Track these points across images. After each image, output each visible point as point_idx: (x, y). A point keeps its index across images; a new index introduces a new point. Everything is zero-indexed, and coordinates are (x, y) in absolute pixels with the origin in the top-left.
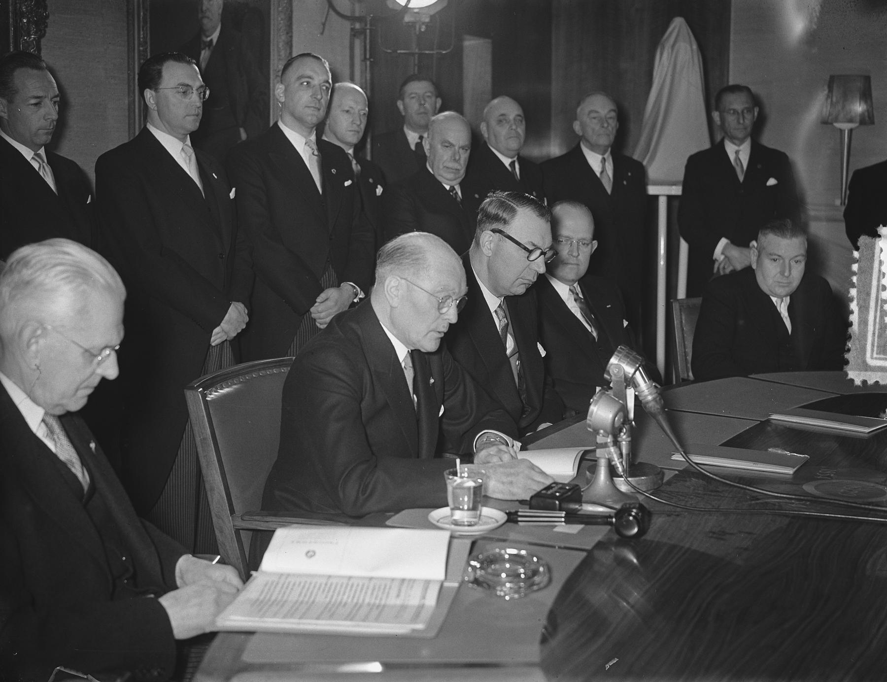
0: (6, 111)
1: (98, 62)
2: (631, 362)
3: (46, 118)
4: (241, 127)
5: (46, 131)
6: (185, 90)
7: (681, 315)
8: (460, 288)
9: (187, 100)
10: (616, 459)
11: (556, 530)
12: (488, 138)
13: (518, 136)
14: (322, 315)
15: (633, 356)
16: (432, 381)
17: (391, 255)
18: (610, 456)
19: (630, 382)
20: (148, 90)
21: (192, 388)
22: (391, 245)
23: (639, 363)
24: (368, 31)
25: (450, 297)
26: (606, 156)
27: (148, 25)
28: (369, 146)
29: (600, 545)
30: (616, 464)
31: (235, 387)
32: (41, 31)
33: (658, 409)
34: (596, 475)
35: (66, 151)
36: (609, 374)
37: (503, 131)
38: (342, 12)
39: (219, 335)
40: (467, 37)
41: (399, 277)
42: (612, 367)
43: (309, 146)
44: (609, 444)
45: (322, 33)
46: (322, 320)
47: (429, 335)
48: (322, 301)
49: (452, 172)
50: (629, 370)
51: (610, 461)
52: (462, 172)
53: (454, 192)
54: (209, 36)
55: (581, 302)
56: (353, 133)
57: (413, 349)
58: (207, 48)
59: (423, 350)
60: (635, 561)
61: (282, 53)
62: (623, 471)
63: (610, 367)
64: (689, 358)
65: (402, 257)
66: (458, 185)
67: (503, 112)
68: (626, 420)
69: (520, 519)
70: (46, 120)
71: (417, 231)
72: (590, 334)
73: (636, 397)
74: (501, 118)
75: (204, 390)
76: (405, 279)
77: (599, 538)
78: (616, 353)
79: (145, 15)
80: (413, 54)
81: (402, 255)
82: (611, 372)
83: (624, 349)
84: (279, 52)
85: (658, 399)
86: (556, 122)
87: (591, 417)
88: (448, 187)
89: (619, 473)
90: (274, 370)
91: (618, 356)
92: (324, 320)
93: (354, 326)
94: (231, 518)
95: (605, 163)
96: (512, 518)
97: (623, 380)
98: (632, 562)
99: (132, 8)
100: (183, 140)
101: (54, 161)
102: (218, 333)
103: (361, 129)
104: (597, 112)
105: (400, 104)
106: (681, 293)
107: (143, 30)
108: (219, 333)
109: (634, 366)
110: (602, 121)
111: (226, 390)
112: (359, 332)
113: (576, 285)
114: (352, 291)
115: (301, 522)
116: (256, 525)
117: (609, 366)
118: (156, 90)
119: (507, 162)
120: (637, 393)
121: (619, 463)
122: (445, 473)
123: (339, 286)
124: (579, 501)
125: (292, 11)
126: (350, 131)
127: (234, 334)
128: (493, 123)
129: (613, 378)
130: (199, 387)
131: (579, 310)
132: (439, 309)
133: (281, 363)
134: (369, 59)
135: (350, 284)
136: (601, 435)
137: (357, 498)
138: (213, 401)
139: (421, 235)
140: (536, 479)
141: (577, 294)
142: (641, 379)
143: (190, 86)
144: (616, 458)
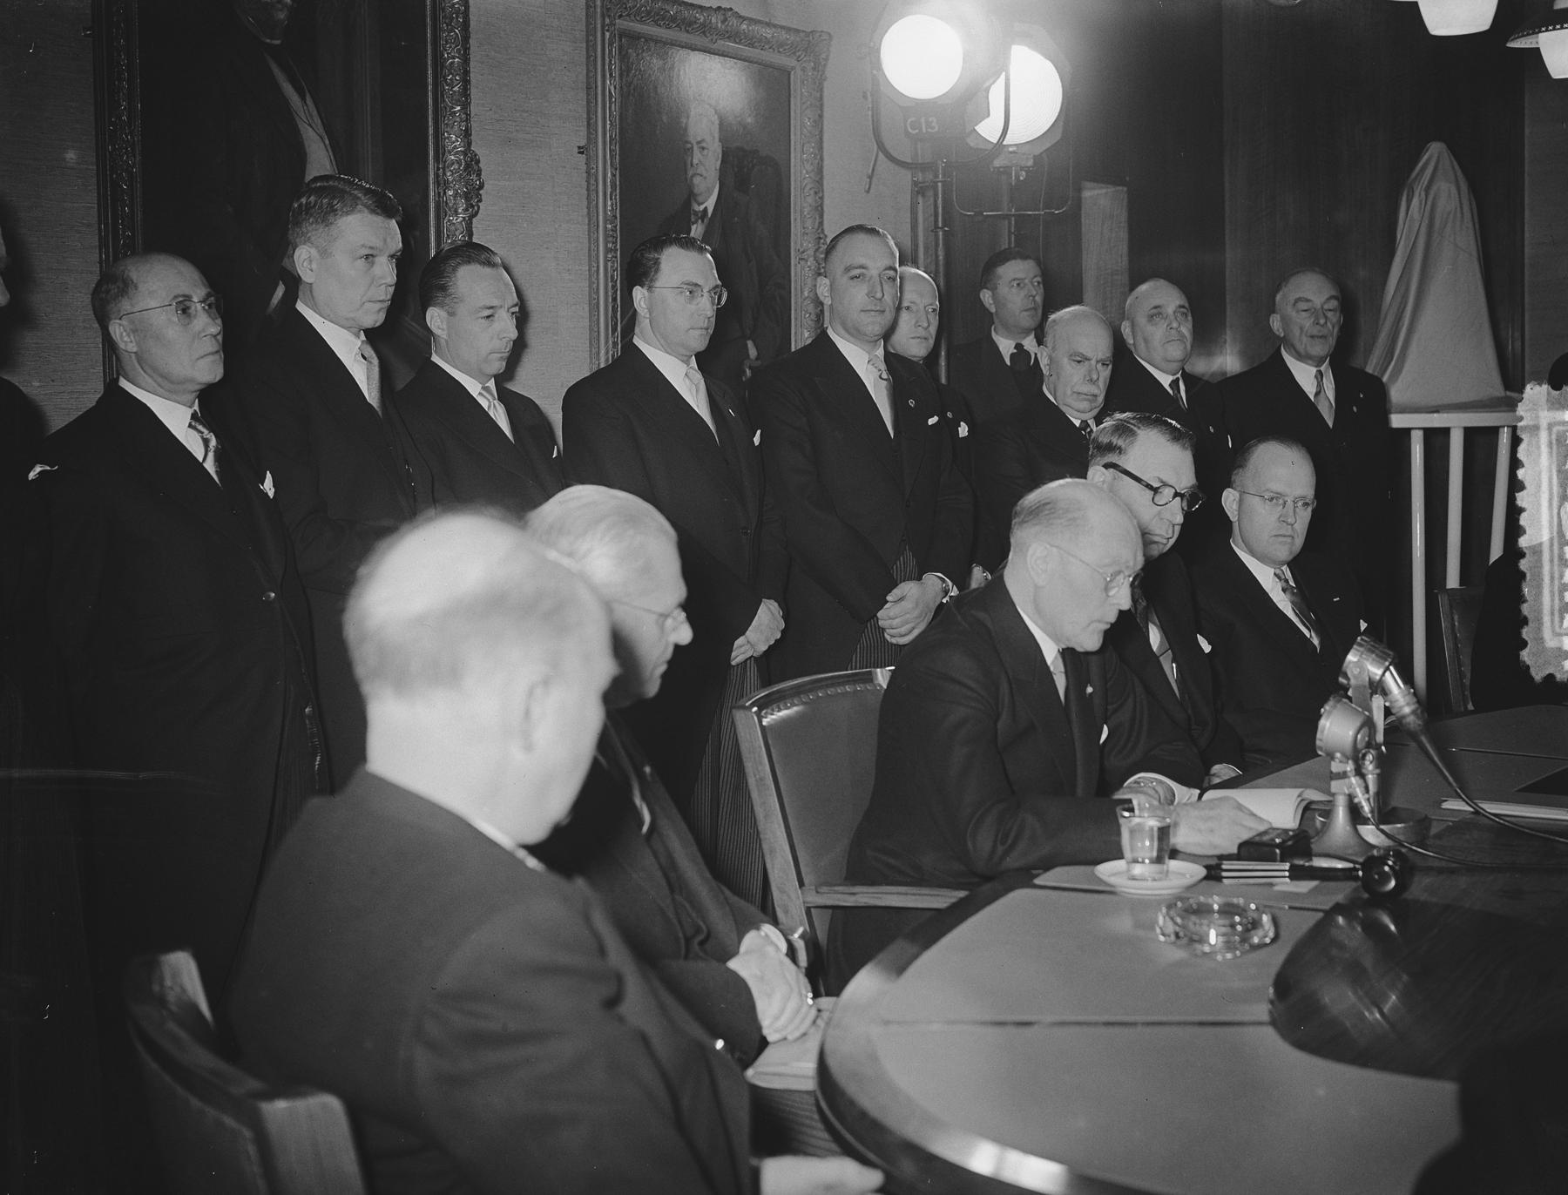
0: (445, 327)
1: (547, 248)
2: (1378, 659)
3: (501, 336)
4: (749, 339)
5: (500, 355)
6: (693, 289)
7: (1452, 613)
8: (1135, 559)
9: (693, 307)
10: (1360, 795)
11: (1277, 888)
12: (1134, 344)
13: (1182, 338)
14: (895, 622)
15: (1381, 651)
16: (1090, 690)
17: (1036, 511)
18: (1351, 790)
19: (1378, 687)
20: (638, 287)
21: (744, 707)
22: (1032, 498)
23: (1390, 660)
24: (940, 184)
25: (1120, 572)
26: (1322, 368)
27: (618, 191)
28: (943, 363)
29: (1338, 909)
30: (1360, 802)
31: (795, 709)
32: (473, 206)
33: (1419, 725)
34: (1331, 820)
35: (514, 387)
36: (1346, 676)
37: (1157, 332)
38: (895, 154)
39: (743, 649)
40: (1088, 184)
41: (1049, 544)
42: (1351, 665)
43: (873, 365)
44: (1349, 774)
45: (868, 191)
46: (894, 631)
47: (1091, 628)
48: (896, 599)
49: (1086, 400)
50: (1376, 671)
51: (1351, 797)
52: (1101, 399)
53: (1089, 430)
54: (702, 204)
55: (1293, 594)
56: (918, 340)
57: (1064, 647)
58: (700, 221)
59: (1079, 649)
60: (1393, 928)
61: (809, 224)
62: (1372, 812)
63: (1347, 667)
64: (1467, 681)
65: (1052, 516)
66: (1092, 420)
67: (1157, 302)
68: (1370, 745)
69: (1224, 874)
70: (501, 339)
71: (1071, 477)
72: (1308, 641)
73: (1388, 712)
74: (1155, 311)
75: (760, 709)
76: (1057, 547)
77: (1340, 898)
78: (1355, 646)
79: (614, 175)
80: (1007, 217)
81: (1053, 513)
82: (1350, 675)
83: (1366, 641)
84: (803, 222)
85: (1419, 711)
86: (1233, 315)
87: (1323, 732)
88: (1077, 423)
89: (1364, 814)
90: (847, 687)
91: (1358, 651)
92: (898, 630)
93: (981, 615)
94: (799, 892)
95: (1322, 380)
96: (1213, 873)
97: (1367, 684)
98: (1387, 927)
99: (595, 166)
100: (687, 362)
101: (505, 396)
102: (741, 647)
103: (930, 334)
104: (1308, 301)
105: (986, 297)
106: (1453, 580)
107: (611, 199)
108: (743, 645)
109: (1383, 664)
110: (1313, 312)
111: (784, 713)
112: (989, 624)
113: (1285, 568)
114: (940, 586)
115: (903, 891)
116: (839, 900)
117: (1345, 665)
118: (650, 288)
119: (1165, 380)
120: (1387, 704)
121: (1365, 801)
122: (1117, 810)
123: (920, 578)
124: (1309, 855)
125: (822, 159)
126: (913, 338)
127: (764, 648)
128: (1141, 320)
129: (1353, 682)
130: (753, 705)
131: (1290, 604)
132: (1107, 589)
133: (856, 678)
134: (942, 228)
135: (938, 577)
136: (1337, 760)
137: (994, 847)
138: (771, 726)
139: (1076, 483)
140: (1245, 823)
141: (1287, 581)
142: (1393, 682)
143: (699, 286)
144: (1359, 792)
